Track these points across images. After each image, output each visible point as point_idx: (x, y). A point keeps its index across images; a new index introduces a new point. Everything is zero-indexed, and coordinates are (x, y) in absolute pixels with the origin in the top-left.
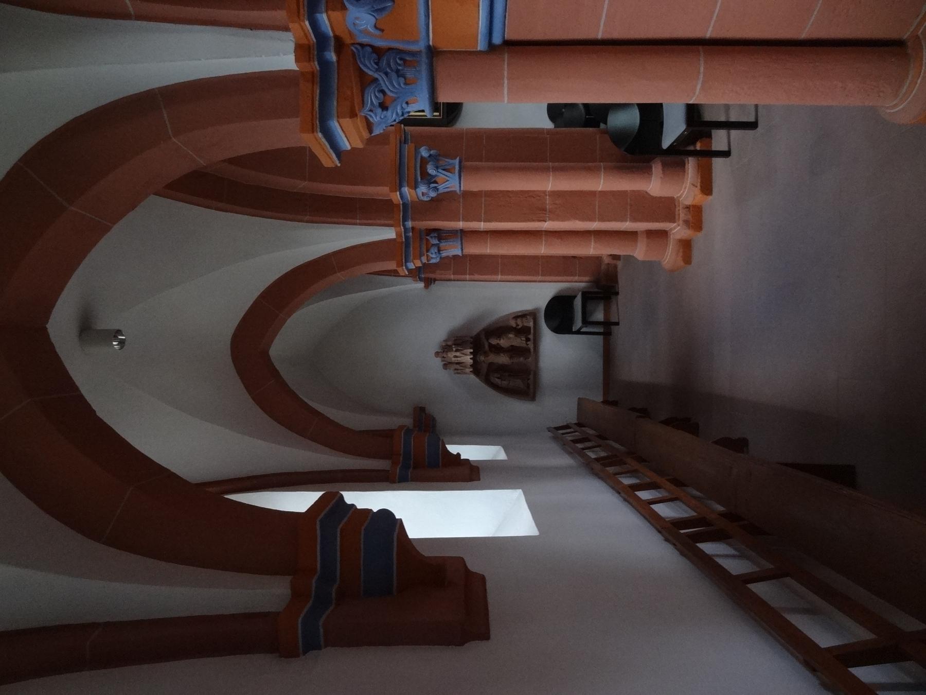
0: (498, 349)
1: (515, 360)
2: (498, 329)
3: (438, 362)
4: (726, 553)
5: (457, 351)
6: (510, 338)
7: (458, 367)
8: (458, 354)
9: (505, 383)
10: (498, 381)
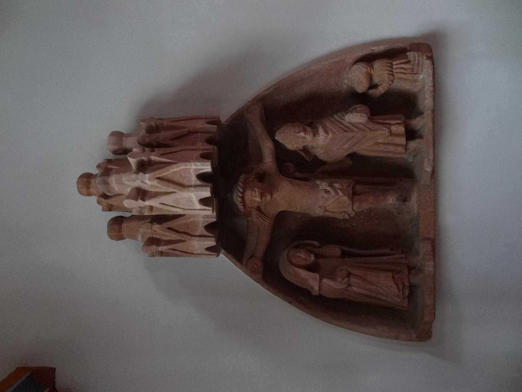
0: (304, 167)
1: (368, 203)
2: (304, 102)
3: (94, 215)
4: (199, 208)
5: (143, 167)
6: (346, 129)
7: (158, 230)
8: (147, 181)
9: (332, 286)
10: (313, 282)
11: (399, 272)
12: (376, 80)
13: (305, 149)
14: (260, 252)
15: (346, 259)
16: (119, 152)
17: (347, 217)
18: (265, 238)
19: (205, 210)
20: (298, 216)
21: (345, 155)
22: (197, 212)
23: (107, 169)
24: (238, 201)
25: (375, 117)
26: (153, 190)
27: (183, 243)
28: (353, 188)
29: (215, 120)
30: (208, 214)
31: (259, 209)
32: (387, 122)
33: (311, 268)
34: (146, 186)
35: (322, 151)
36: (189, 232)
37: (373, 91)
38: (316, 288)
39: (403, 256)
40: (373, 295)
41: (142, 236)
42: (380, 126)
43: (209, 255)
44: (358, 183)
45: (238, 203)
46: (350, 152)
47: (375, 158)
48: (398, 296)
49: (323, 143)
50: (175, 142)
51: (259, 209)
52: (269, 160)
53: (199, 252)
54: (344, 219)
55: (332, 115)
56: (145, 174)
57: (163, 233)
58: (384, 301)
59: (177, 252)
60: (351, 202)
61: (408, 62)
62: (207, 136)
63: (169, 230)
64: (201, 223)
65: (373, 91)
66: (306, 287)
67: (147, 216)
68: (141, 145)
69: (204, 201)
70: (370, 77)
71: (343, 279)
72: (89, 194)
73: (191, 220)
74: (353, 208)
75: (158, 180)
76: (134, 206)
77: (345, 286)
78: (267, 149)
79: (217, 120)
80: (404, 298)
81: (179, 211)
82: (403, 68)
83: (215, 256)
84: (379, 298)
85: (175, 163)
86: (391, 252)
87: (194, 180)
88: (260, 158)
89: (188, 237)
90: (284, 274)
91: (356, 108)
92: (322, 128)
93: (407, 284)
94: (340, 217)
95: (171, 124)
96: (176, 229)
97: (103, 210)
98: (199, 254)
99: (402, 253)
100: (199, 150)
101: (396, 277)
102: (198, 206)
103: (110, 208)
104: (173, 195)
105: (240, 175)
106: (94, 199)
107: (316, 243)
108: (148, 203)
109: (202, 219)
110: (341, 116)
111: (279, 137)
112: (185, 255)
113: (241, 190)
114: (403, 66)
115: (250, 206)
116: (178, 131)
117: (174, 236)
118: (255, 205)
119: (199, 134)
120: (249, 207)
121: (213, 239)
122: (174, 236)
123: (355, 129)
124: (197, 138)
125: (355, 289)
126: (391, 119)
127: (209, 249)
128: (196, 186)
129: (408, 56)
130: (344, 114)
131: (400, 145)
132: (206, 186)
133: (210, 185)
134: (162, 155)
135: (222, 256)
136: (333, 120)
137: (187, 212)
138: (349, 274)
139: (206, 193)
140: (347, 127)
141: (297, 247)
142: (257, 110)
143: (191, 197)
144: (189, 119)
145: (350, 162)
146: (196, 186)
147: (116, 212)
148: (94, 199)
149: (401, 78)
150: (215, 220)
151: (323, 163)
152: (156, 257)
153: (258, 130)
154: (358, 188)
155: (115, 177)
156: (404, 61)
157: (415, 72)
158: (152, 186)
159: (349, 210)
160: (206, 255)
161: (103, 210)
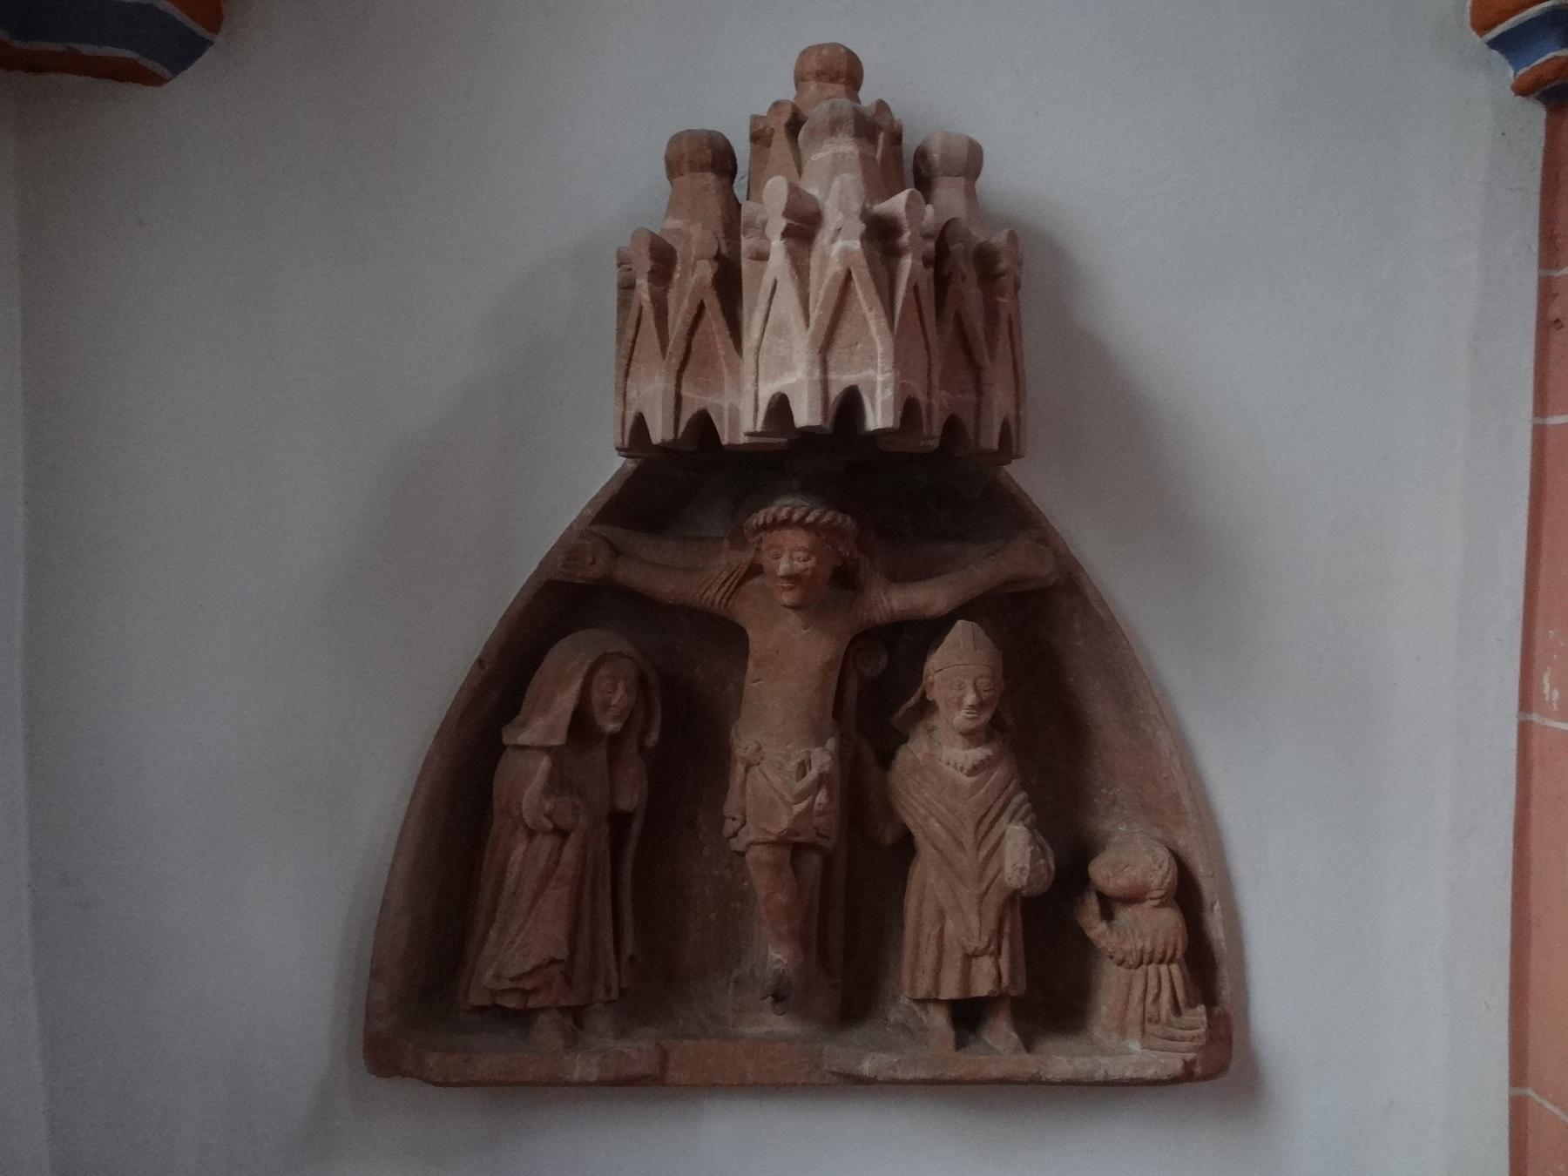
3: (739, 93)
8: (840, 244)
9: (527, 782)
10: (542, 725)
11: (568, 979)
12: (1125, 915)
13: (926, 708)
14: (631, 574)
15: (605, 829)
17: (730, 827)
18: (667, 587)
19: (756, 410)
21: (910, 822)
22: (748, 387)
23: (873, 128)
26: (814, 262)
27: (658, 349)
28: (812, 847)
29: (1014, 443)
31: (755, 570)
33: (581, 723)
35: (919, 756)
36: (690, 367)
37: (1093, 904)
38: (524, 738)
39: (614, 995)
42: (991, 925)
44: (828, 861)
48: (498, 977)
50: (950, 328)
51: (755, 570)
52: (896, 600)
53: (632, 394)
55: (1023, 786)
57: (689, 289)
59: (630, 332)
60: (772, 838)
61: (1176, 1009)
62: (967, 417)
66: (525, 707)
69: (780, 407)
70: (1133, 898)
71: (548, 816)
72: (800, 79)
73: (725, 370)
75: (842, 277)
77: (528, 820)
78: (929, 597)
79: (1014, 450)
80: (493, 993)
81: (751, 336)
82: (1158, 995)
87: (841, 380)
89: (675, 362)
90: (564, 643)
91: (1044, 856)
94: (731, 807)
96: (700, 329)
97: (755, 119)
99: (622, 992)
100: (929, 395)
102: (767, 391)
103: (760, 138)
106: (788, 92)
107: (653, 738)
108: (777, 246)
109: (726, 405)
113: (810, 519)
114: (1166, 995)
117: (678, 322)
118: (766, 560)
119: (974, 399)
121: (670, 437)
122: (678, 322)
123: (984, 853)
127: (640, 424)
128: (825, 383)
135: (617, 463)
136: (1011, 787)
138: (562, 834)
141: (642, 682)
145: (888, 838)
146: (825, 383)
149: (1130, 986)
150: (725, 440)
151: (886, 760)
153: (983, 569)
154: (814, 862)
156: (1181, 995)
157: (1150, 1028)
158: (825, 258)
159: (751, 834)
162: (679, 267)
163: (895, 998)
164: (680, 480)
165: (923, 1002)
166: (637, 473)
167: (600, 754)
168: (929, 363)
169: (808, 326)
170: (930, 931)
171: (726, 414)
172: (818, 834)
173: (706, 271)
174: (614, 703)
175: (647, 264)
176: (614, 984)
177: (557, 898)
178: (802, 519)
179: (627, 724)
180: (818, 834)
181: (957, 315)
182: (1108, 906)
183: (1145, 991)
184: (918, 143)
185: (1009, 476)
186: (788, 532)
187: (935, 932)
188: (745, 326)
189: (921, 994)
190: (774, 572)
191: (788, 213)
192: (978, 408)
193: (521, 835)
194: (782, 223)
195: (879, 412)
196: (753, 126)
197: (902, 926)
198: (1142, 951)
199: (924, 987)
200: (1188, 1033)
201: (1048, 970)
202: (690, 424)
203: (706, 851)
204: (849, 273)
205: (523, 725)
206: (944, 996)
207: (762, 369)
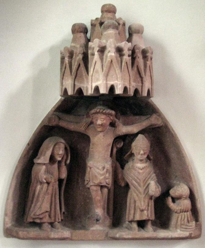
3: (89, 14)
5: (119, 51)
8: (111, 54)
9: (41, 170)
10: (43, 159)
11: (50, 216)
12: (177, 202)
13: (132, 155)
14: (63, 124)
15: (57, 182)
16: (130, 31)
17: (86, 182)
18: (72, 127)
19: (92, 89)
20: (86, 150)
21: (128, 181)
22: (90, 83)
23: (119, 25)
24: (97, 110)
25: (153, 201)
26: (104, 57)
27: (70, 73)
28: (105, 187)
29: (151, 94)
30: (89, 91)
31: (92, 123)
32: (150, 208)
33: (52, 159)
34: (107, 52)
35: (130, 166)
36: (77, 77)
37: (170, 199)
38: (39, 161)
39: (60, 220)
40: (35, 199)
41: (74, 47)
42: (147, 204)
43: (62, 90)
44: (109, 190)
45: (96, 109)
46: (130, 184)
47: (126, 202)
48: (34, 215)
49: (136, 166)
50: (135, 69)
51: (92, 123)
52: (124, 129)
53: (64, 83)
54: (84, 180)
55: (155, 173)
56: (114, 53)
57: (76, 60)
58: (31, 206)
59: (64, 69)
60: (96, 184)
61: (188, 222)
62: (140, 89)
63: (78, 64)
64: (83, 85)
65: (170, 199)
66: (39, 154)
67: (88, 52)
68: (134, 47)
69: (97, 89)
70: (179, 198)
71: (45, 179)
72: (102, 12)
73: (85, 78)
74: (92, 186)
75: (110, 61)
76: (95, 44)
77: (40, 180)
78: (132, 129)
79: (151, 96)
80: (33, 219)
81: (91, 72)
82: (184, 219)
83: (61, 94)
84: (32, 203)
85: (121, 71)
86: (62, 213)
87: (110, 83)
88: (126, 124)
89: (74, 77)
90: (48, 140)
91: (158, 188)
92: (146, 166)
93: (42, 221)
94: (87, 178)
95: (148, 66)
96: (79, 69)
97: (92, 21)
98: (62, 83)
99: (62, 220)
100: (130, 86)
101: (47, 214)
102: (94, 85)
103: (93, 25)
104: (101, 69)
105: (114, 111)
106: (99, 15)
107: (68, 162)
108: (96, 53)
109: (85, 86)
110: (154, 178)
111: (140, 136)
112: (62, 74)
113: (104, 112)
114: (186, 219)
115: (94, 117)
116: (143, 70)
117: (74, 67)
118: (94, 121)
119: (141, 84)
120: (93, 116)
121: (72, 94)
122: (74, 67)
123: (145, 187)
124: (138, 83)
125: (39, 187)
126: (151, 212)
127: (66, 91)
128: (107, 84)
129: (192, 222)
130: (155, 180)
131: (134, 217)
132: (107, 91)
133: (107, 93)
134: (127, 63)
135: (60, 97)
136: (151, 173)
137: (90, 78)
138: (48, 183)
139: (103, 90)
140: (146, 182)
141: (66, 148)
142: (159, 123)
143: (100, 80)
144: (151, 78)
145: (123, 185)
146: (107, 84)
147: (90, 28)
148: (99, 15)
149: (178, 218)
150: (85, 94)
151: (123, 167)
152: (60, 55)
153: (144, 123)
154: (106, 190)
155: (113, 33)
156: (189, 219)
157: (183, 226)
158: (107, 56)
159: (91, 183)
160: (62, 89)
161: (92, 21)
162: (74, 55)
163: (125, 222)
164: (74, 104)
165: (131, 222)
166: (64, 100)
167: (56, 166)
168: (130, 79)
169: (103, 71)
170: (132, 205)
171: (85, 88)
172: (107, 184)
173: (81, 56)
174: (60, 152)
175: (68, 55)
176: (60, 218)
177: (48, 198)
178: (102, 112)
179: (62, 158)
180: (107, 184)
181: (137, 66)
182: (174, 200)
183: (182, 218)
184: (130, 25)
185: (151, 101)
186: (99, 115)
187: (134, 205)
188: (89, 71)
189: (130, 220)
190: (96, 124)
191: (99, 47)
192: (142, 86)
193: (39, 183)
194: (98, 49)
195: (118, 90)
196: (91, 22)
197: (126, 207)
198: (181, 209)
199: (131, 217)
200: (190, 227)
201: (162, 216)
202: (77, 90)
203: (81, 188)
204: (112, 61)
205: (39, 158)
206: (136, 219)
207: (93, 80)
